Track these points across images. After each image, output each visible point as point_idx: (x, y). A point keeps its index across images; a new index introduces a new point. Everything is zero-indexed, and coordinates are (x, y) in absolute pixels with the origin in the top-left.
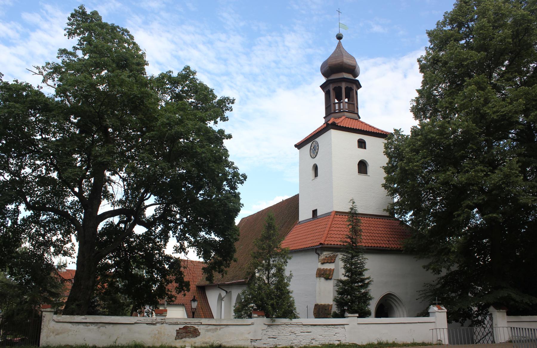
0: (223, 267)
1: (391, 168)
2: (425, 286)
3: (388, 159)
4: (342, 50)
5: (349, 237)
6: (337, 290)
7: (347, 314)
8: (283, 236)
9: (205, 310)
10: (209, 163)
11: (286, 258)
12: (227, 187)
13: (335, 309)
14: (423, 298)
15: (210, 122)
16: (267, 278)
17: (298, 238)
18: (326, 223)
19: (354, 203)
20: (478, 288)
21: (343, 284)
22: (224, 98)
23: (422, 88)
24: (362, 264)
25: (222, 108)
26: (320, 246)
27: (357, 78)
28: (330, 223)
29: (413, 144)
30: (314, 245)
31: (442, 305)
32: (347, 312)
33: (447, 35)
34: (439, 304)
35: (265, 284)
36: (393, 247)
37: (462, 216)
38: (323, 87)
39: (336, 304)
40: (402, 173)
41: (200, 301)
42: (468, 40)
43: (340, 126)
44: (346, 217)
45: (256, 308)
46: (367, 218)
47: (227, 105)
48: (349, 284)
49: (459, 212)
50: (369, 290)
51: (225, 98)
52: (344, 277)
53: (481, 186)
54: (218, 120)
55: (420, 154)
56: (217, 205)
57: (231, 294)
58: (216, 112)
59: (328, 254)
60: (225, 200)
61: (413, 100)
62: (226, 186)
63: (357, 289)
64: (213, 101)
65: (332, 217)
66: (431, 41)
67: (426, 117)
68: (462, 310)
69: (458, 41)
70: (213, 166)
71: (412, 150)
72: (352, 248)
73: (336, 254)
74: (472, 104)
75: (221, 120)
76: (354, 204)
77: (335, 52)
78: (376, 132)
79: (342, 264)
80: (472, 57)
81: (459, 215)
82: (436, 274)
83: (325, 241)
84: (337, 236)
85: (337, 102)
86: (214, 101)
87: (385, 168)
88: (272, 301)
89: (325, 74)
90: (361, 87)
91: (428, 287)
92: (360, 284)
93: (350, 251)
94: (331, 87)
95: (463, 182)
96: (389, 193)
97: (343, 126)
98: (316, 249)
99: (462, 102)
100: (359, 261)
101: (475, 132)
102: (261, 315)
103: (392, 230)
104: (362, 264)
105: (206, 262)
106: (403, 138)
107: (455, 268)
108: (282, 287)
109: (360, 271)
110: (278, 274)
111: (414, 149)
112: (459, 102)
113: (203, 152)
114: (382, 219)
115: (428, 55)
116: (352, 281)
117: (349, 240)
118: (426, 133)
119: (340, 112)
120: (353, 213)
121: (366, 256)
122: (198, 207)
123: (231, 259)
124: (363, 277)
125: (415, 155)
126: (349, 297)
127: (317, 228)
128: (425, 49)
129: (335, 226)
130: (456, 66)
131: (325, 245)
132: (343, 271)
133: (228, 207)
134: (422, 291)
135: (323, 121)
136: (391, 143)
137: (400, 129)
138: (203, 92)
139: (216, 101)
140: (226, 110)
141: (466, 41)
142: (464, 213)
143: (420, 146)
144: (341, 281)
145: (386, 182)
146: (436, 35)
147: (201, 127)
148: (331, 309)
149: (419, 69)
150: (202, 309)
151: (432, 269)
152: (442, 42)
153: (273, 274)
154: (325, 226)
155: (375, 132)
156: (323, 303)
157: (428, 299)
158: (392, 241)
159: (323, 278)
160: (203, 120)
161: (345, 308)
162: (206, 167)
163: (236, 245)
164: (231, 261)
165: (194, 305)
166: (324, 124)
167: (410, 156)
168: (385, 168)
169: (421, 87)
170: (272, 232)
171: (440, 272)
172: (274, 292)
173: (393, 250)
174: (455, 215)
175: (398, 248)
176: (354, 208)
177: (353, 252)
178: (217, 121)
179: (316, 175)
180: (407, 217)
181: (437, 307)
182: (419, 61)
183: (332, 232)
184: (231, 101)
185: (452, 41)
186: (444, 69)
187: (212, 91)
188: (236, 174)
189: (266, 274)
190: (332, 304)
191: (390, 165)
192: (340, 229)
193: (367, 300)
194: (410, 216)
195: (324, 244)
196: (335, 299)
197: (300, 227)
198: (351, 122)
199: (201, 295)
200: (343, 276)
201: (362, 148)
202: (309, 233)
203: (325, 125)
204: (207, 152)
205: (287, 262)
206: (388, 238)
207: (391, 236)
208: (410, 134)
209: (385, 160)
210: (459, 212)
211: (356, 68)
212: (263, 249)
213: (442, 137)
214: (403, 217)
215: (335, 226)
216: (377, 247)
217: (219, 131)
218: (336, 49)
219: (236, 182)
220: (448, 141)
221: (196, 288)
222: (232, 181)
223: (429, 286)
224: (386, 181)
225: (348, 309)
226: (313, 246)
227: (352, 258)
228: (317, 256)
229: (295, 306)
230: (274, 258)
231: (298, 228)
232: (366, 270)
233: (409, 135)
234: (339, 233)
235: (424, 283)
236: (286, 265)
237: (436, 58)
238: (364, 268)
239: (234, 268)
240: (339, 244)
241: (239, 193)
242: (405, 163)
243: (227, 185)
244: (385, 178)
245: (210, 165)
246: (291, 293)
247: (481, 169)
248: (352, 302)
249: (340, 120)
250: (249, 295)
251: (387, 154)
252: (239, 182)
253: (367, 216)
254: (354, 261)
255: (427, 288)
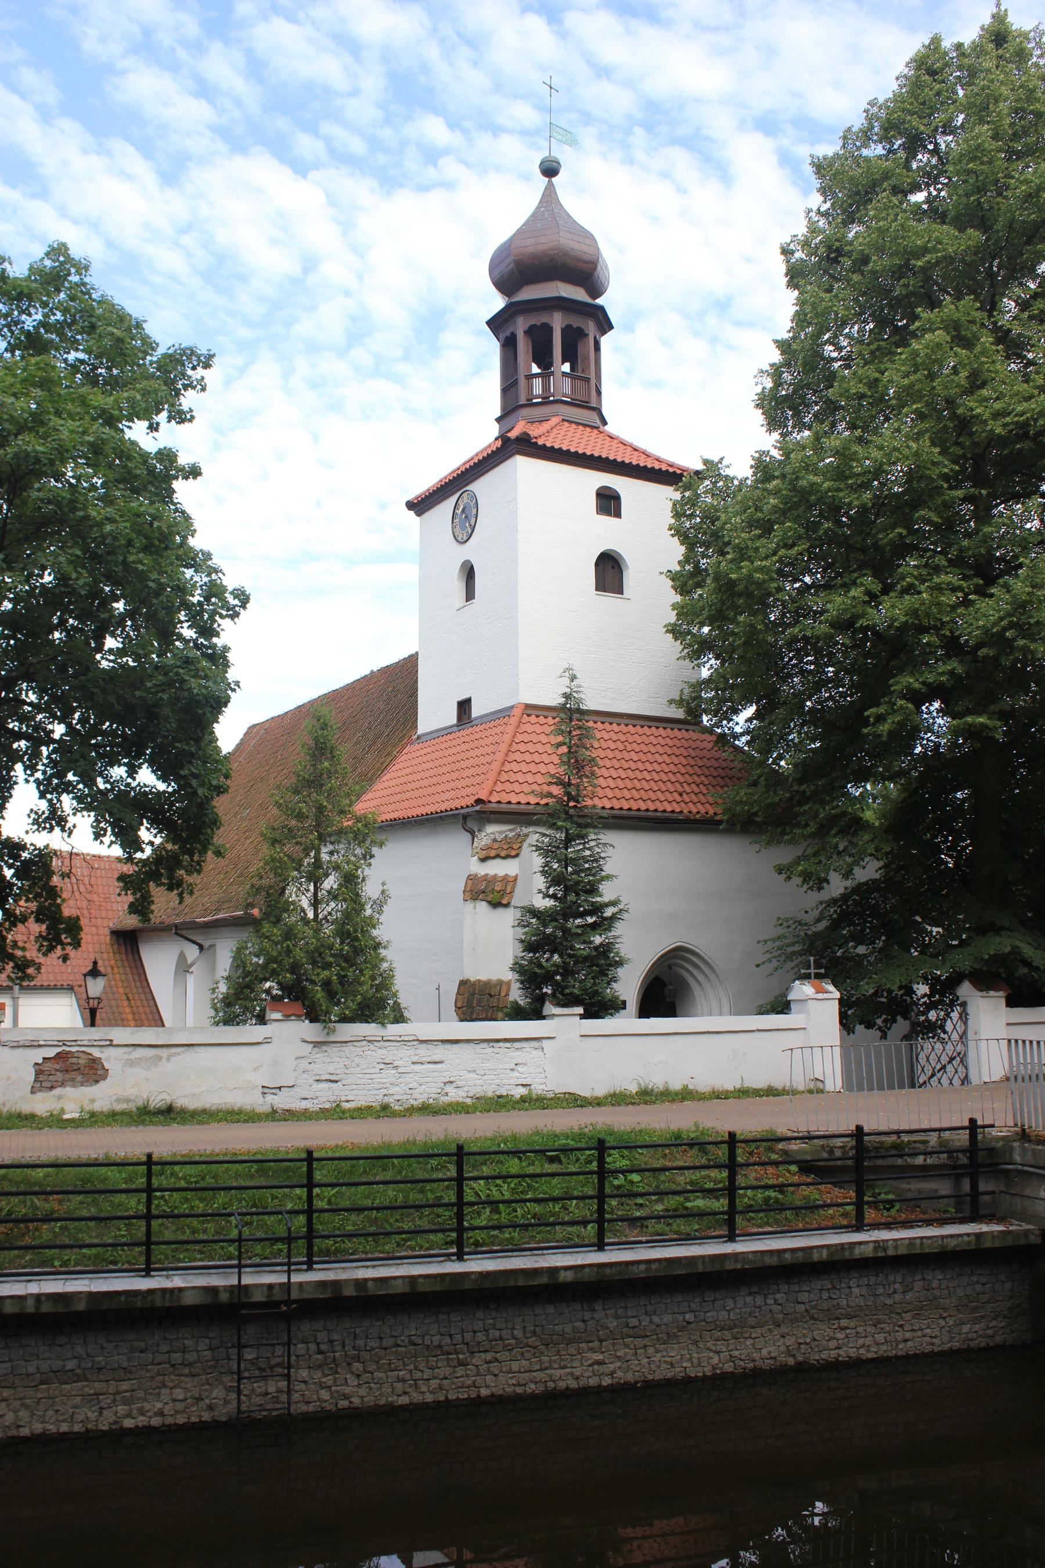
0: (182, 872)
1: (692, 575)
2: (781, 925)
3: (683, 548)
4: (556, 210)
5: (559, 783)
6: (523, 937)
7: (549, 1008)
8: (369, 779)
9: (139, 1003)
10: (129, 552)
11: (368, 842)
12: (189, 627)
13: (516, 995)
14: (775, 963)
15: (131, 424)
16: (311, 905)
17: (413, 786)
18: (496, 738)
19: (573, 678)
20: (931, 931)
21: (538, 918)
22: (181, 349)
23: (791, 335)
24: (596, 861)
25: (174, 382)
26: (478, 808)
27: (599, 301)
28: (507, 738)
29: (754, 504)
30: (457, 803)
31: (826, 980)
32: (551, 1002)
33: (872, 174)
34: (818, 976)
35: (305, 921)
36: (694, 810)
37: (889, 721)
38: (496, 324)
39: (518, 980)
40: (720, 590)
41: (123, 977)
42: (934, 193)
43: (544, 445)
44: (550, 721)
45: (280, 993)
46: (619, 725)
47: (190, 372)
48: (556, 920)
49: (881, 710)
50: (615, 937)
51: (184, 350)
52: (544, 898)
53: (948, 633)
54: (162, 417)
55: (775, 536)
56: (156, 685)
57: (215, 952)
58: (149, 392)
59: (500, 833)
60: (179, 667)
61: (762, 372)
62: (186, 625)
63: (580, 935)
64: (144, 359)
65: (514, 721)
66: (823, 191)
67: (801, 426)
68: (885, 994)
69: (905, 193)
70: (141, 562)
71: (752, 524)
72: (567, 813)
73: (525, 830)
74: (934, 388)
75: (170, 419)
76: (575, 682)
77: (534, 216)
78: (653, 468)
79: (538, 861)
80: (940, 243)
81: (880, 719)
82: (811, 888)
83: (491, 793)
84: (530, 778)
85: (539, 371)
86: (149, 358)
87: (674, 577)
88: (327, 973)
89: (505, 283)
90: (611, 327)
91: (791, 929)
92: (590, 920)
93: (560, 824)
94: (521, 325)
95: (896, 620)
96: (686, 651)
97: (552, 447)
98: (465, 817)
99: (906, 381)
100: (588, 853)
101: (937, 471)
102: (294, 1015)
103: (693, 763)
104: (596, 861)
105: (130, 859)
106: (728, 488)
107: (869, 871)
108: (356, 931)
109: (590, 881)
110: (343, 893)
111: (758, 521)
112: (895, 379)
113: (107, 519)
114: (665, 728)
115: (813, 232)
116: (569, 911)
117: (556, 790)
118: (794, 473)
119: (546, 402)
120: (570, 709)
121: (608, 837)
122: (96, 691)
123: (204, 851)
124: (599, 899)
125: (760, 537)
126: (556, 957)
127: (468, 755)
128: (804, 215)
129: (522, 747)
130: (895, 269)
131: (491, 805)
132: (540, 882)
133: (189, 690)
134: (773, 940)
135: (494, 430)
136: (693, 502)
137: (722, 459)
138: (110, 329)
139: (155, 359)
140: (186, 387)
141: (930, 194)
142: (895, 711)
143: (775, 509)
144: (533, 912)
145: (678, 620)
146: (837, 172)
147: (102, 440)
148: (507, 995)
149: (786, 275)
150: (128, 999)
151: (800, 876)
152: (857, 193)
153: (329, 892)
154: (492, 748)
155: (649, 466)
156: (484, 977)
157: (793, 964)
158: (693, 795)
159: (484, 903)
160: (111, 421)
161: (545, 990)
162: (117, 566)
163: (221, 805)
164: (206, 853)
165: (96, 987)
166: (496, 439)
167: (744, 540)
168: (674, 577)
169: (789, 331)
170: (326, 764)
171: (825, 885)
172: (331, 947)
173: (677, 821)
174: (869, 717)
175: (707, 813)
176: (575, 695)
177: (569, 825)
178: (158, 424)
179: (470, 595)
180: (737, 724)
181: (814, 987)
182: (786, 252)
183: (515, 767)
184: (202, 358)
185: (885, 190)
186: (856, 277)
187: (139, 325)
188: (214, 591)
189: (308, 891)
190: (510, 978)
191: (687, 567)
192: (537, 758)
193: (611, 965)
194: (746, 721)
195: (490, 802)
196: (516, 964)
197: (422, 752)
198: (578, 435)
199: (124, 956)
200: (541, 895)
201: (610, 515)
202: (444, 769)
203: (499, 444)
204: (121, 516)
205: (372, 856)
206: (681, 783)
207: (690, 780)
208: (749, 473)
209: (674, 552)
210: (881, 710)
211: (599, 268)
212: (300, 816)
213: (842, 486)
214: (725, 722)
215: (522, 747)
216: (647, 810)
217: (160, 452)
218: (538, 208)
219: (213, 614)
220: (857, 499)
221: (108, 938)
222: (205, 611)
223: (793, 926)
224: (677, 614)
225: (554, 995)
226: (457, 809)
227: (568, 841)
228: (468, 836)
229: (397, 988)
230: (332, 843)
231: (414, 755)
232: (609, 877)
233: (747, 478)
234: (533, 768)
235: (779, 919)
236: (370, 865)
237: (837, 244)
238: (603, 873)
239: (222, 876)
240: (523, 802)
241: (226, 649)
242: (732, 561)
243: (187, 621)
244: (674, 606)
245: (131, 558)
246: (385, 948)
247: (949, 583)
248: (567, 972)
249: (546, 426)
250: (258, 956)
251: (679, 532)
252: (224, 613)
253: (619, 720)
254: (572, 852)
255: (786, 930)
